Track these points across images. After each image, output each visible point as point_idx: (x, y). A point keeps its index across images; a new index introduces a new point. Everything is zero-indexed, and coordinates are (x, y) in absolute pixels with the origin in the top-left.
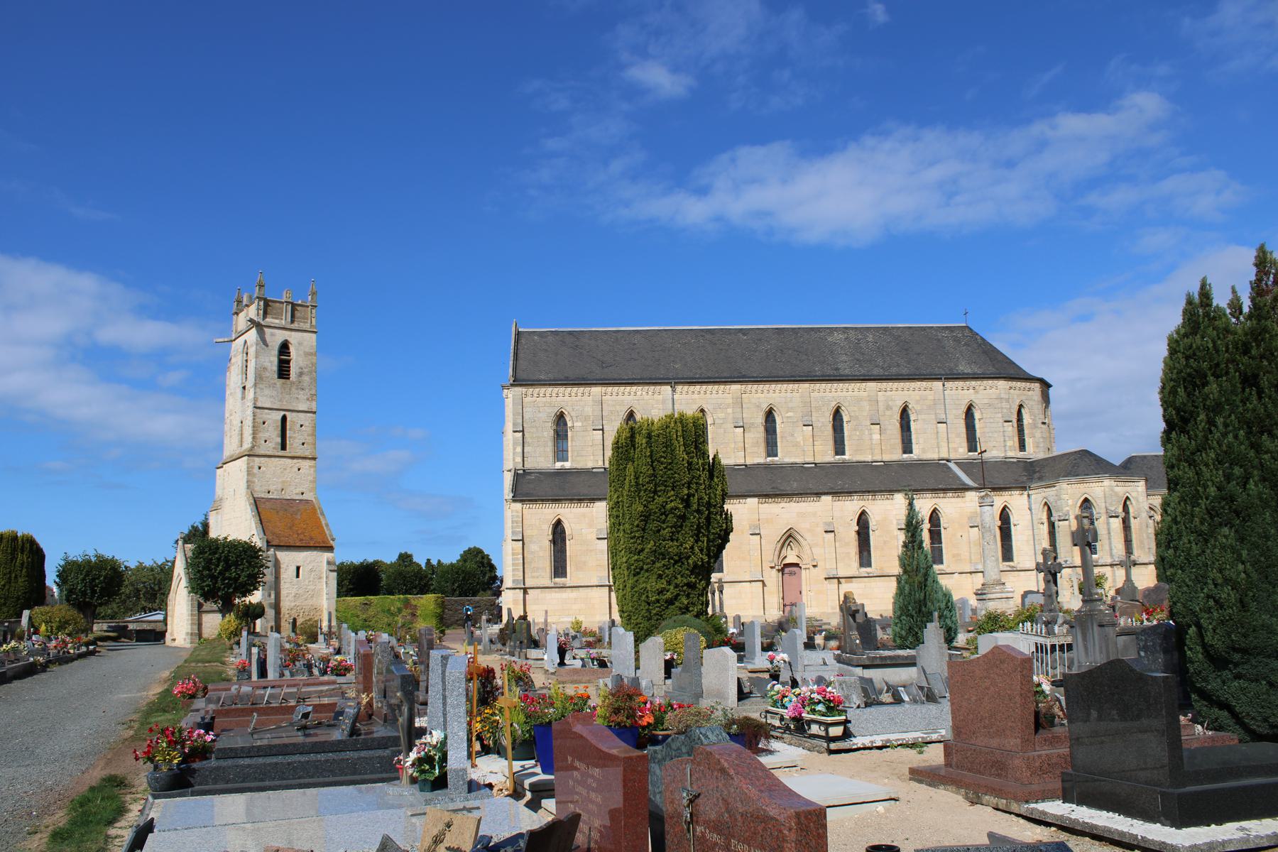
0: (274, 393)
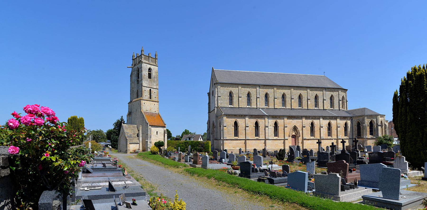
0: (148, 83)
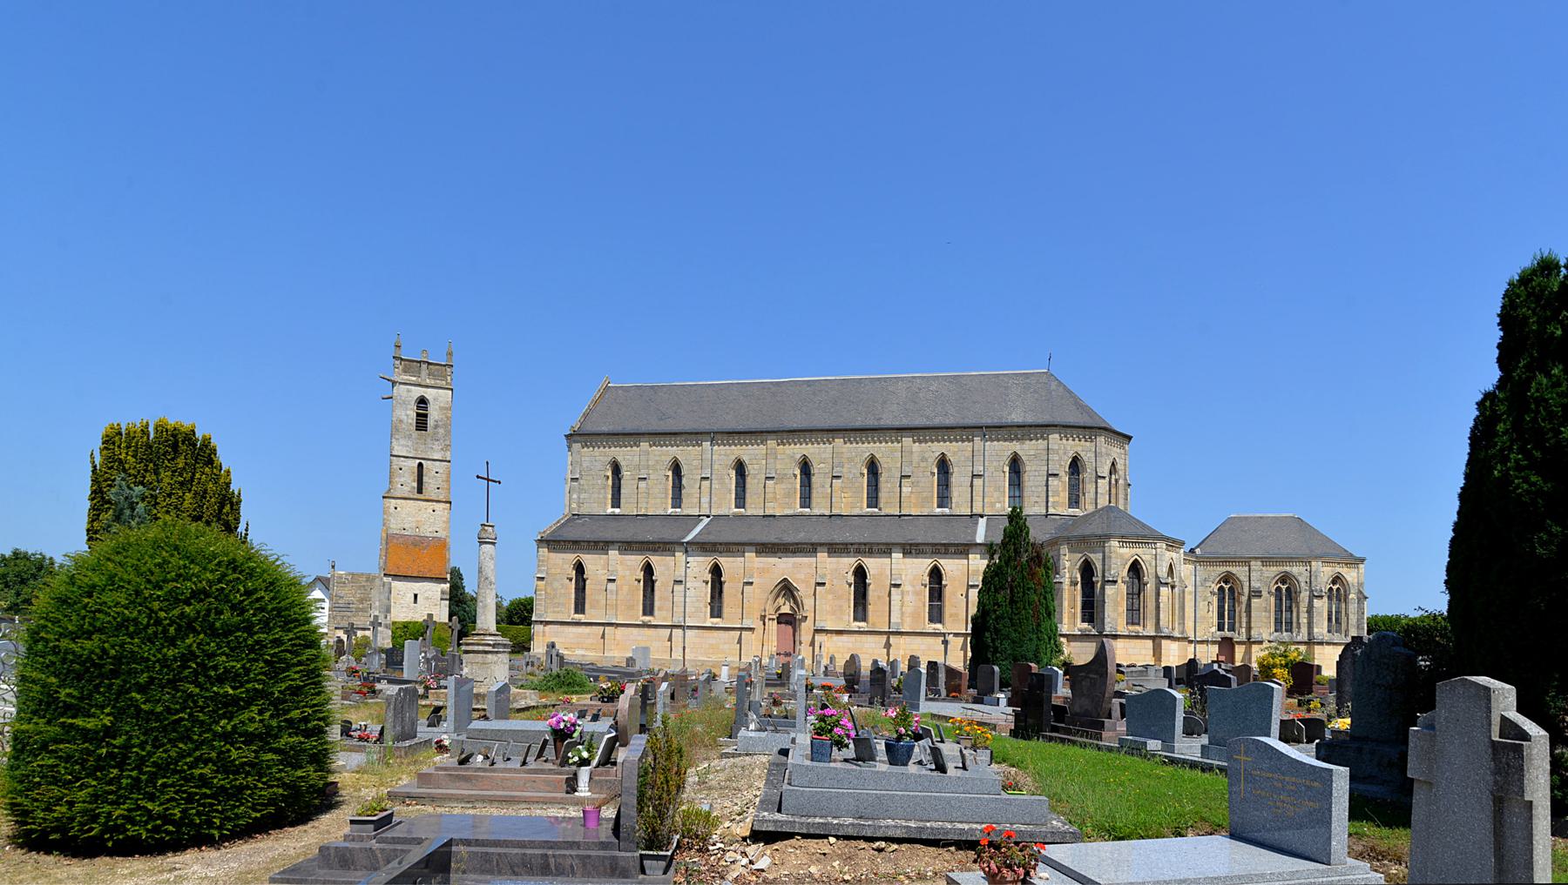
0: (410, 443)
